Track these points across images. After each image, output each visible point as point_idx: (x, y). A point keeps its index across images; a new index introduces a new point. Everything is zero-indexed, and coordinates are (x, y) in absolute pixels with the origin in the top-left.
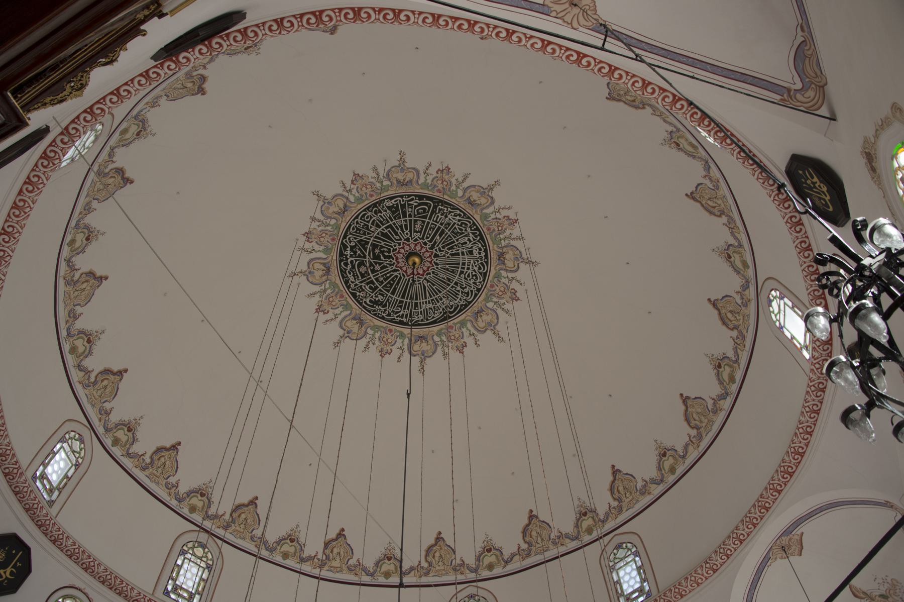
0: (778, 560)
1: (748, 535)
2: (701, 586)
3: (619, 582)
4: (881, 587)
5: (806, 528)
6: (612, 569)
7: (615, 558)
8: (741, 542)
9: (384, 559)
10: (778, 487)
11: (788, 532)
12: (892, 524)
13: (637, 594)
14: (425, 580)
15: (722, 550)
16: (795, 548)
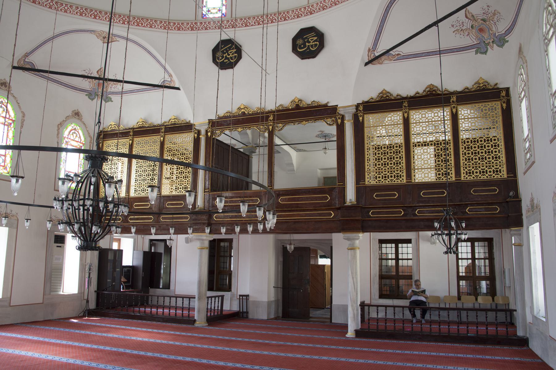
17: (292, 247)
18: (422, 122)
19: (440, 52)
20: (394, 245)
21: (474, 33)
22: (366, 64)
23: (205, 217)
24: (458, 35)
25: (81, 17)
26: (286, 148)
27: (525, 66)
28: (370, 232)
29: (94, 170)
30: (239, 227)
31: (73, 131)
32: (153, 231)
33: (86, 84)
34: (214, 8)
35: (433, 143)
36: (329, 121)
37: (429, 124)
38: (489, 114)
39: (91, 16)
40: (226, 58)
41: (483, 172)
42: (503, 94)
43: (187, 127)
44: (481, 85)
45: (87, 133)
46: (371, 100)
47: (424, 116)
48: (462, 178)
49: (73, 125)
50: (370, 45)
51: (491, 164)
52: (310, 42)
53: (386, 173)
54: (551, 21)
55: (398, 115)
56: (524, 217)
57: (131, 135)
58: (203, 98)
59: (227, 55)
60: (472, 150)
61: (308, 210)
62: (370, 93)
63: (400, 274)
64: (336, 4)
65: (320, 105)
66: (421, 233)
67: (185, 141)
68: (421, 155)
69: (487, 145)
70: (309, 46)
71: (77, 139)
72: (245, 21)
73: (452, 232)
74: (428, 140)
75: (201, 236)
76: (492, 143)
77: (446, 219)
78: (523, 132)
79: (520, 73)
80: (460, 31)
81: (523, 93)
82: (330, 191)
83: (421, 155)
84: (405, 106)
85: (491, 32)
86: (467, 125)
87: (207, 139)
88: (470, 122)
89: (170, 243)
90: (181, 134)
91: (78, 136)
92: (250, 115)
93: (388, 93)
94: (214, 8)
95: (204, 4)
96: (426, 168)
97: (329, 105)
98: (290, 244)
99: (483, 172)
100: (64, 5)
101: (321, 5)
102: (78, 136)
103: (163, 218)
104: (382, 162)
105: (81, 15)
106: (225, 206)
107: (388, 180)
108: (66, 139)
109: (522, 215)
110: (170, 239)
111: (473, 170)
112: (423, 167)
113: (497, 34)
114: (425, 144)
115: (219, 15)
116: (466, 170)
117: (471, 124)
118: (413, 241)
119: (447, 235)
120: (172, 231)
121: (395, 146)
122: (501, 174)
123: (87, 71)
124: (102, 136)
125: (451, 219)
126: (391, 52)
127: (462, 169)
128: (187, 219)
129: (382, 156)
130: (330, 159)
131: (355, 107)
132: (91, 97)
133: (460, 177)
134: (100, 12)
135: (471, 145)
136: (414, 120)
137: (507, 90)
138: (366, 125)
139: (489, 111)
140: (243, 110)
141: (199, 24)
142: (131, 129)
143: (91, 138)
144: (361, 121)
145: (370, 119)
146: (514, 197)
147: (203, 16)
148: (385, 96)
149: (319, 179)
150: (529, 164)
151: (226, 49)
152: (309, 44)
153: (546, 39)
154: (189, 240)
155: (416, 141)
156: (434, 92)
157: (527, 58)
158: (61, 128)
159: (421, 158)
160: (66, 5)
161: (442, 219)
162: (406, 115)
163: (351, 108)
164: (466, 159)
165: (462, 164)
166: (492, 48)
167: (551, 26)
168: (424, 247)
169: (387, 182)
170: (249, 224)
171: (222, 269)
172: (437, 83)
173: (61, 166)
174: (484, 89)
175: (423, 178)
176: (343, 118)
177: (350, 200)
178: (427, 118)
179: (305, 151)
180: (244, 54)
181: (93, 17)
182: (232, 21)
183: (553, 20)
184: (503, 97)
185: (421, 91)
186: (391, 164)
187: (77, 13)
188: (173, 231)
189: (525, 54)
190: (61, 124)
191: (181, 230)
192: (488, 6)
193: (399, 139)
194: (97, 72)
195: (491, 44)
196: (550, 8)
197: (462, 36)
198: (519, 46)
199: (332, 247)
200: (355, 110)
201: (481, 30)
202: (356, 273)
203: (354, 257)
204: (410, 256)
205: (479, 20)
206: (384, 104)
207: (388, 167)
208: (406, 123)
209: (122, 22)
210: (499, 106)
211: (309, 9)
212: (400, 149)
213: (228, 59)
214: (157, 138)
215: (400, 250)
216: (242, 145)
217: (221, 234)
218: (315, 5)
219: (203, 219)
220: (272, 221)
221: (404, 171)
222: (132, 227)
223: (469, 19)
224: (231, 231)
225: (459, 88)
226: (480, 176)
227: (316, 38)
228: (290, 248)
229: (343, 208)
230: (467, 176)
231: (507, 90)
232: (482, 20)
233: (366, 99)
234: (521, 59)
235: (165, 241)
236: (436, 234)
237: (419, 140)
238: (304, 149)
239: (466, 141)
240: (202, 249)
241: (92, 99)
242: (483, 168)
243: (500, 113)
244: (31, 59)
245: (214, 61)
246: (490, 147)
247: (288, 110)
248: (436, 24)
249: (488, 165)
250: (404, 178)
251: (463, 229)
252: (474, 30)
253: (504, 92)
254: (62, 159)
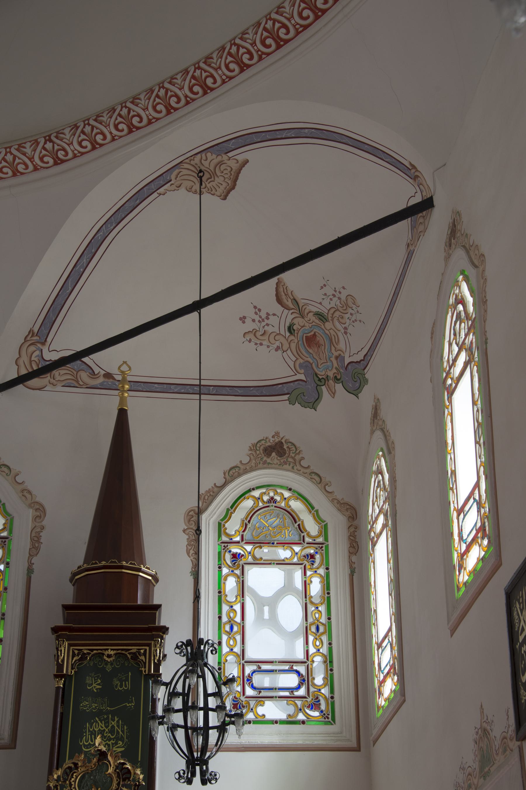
0: (182, 190)
1: (150, 122)
2: (20, 179)
4: (326, 303)
5: (257, 156)
8: (131, 129)
10: (245, 58)
11: (222, 147)
12: (400, 206)
15: (88, 129)
16: (220, 182)
19: (200, 390)
79: (375, 468)
183: (466, 335)
196: (460, 307)
198: (26, 565)
201: (311, 340)
248: (197, 306)
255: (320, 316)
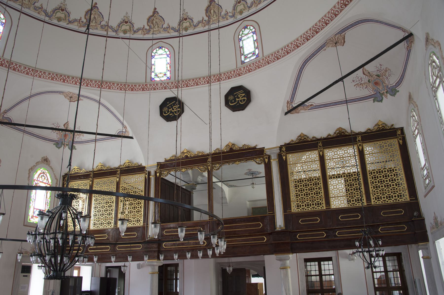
3: (242, 47)
6: (240, 40)
7: (242, 34)
9: (236, 4)
13: (251, 55)
14: (147, 36)
17: (231, 269)
18: (335, 159)
19: (346, 102)
20: (317, 263)
21: (371, 86)
22: (286, 114)
23: (155, 246)
24: (358, 88)
25: (52, 81)
26: (220, 184)
27: (416, 109)
28: (296, 253)
29: (65, 207)
30: (190, 253)
31: (42, 174)
32: (113, 259)
33: (54, 135)
34: (161, 73)
35: (335, 176)
36: (258, 160)
37: (341, 160)
38: (389, 150)
39: (60, 80)
40: (171, 112)
41: (390, 197)
42: (399, 132)
43: (140, 169)
44: (381, 126)
45: (53, 175)
46: (292, 142)
47: (336, 153)
48: (373, 203)
49: (42, 169)
50: (288, 98)
51: (396, 190)
52: (239, 98)
53: (309, 201)
54: (437, 73)
55: (315, 153)
56: (429, 233)
57: (91, 177)
58: (154, 145)
59: (171, 109)
60: (378, 180)
61: (244, 236)
62: (291, 136)
63: (324, 288)
64: (259, 68)
65: (250, 148)
66: (339, 251)
67: (136, 182)
68: (336, 186)
69: (390, 175)
70: (238, 101)
71: (45, 181)
72: (186, 82)
73: (371, 249)
74: (352, 171)
75: (152, 262)
76: (383, 174)
77: (364, 238)
78: (420, 162)
79: (411, 115)
80: (359, 85)
81: (417, 131)
82: (262, 219)
83: (336, 186)
84: (320, 146)
85: (384, 84)
86: (372, 159)
87: (156, 179)
88: (374, 156)
89: (124, 269)
90: (134, 175)
91: (46, 178)
92: (192, 157)
93: (305, 136)
94: (161, 73)
95: (153, 70)
96: (342, 196)
97: (257, 147)
98: (229, 266)
99: (390, 197)
100: (39, 72)
101: (248, 68)
102: (46, 178)
103: (119, 248)
104: (304, 192)
105: (52, 79)
106: (185, 234)
107: (311, 207)
108: (36, 182)
109: (426, 231)
110: (124, 266)
111: (381, 195)
112: (339, 195)
113: (389, 86)
114: (339, 176)
115: (165, 78)
116: (375, 196)
117: (375, 158)
118: (333, 259)
119: (367, 252)
120: (130, 259)
121: (314, 179)
122: (404, 198)
123: (55, 124)
124: (66, 179)
125: (369, 238)
126: (306, 103)
127: (371, 195)
128: (139, 248)
129: (304, 188)
130: (259, 192)
131: (278, 149)
132: (58, 146)
133: (371, 202)
134: (68, 77)
135: (377, 175)
136: (328, 157)
137: (402, 129)
138: (288, 163)
139: (389, 147)
140: (186, 154)
141: (149, 85)
142: (91, 172)
143: (57, 180)
144: (284, 159)
145: (291, 158)
146: (418, 217)
147: (152, 79)
148: (303, 138)
149: (248, 210)
150: (429, 188)
151: (171, 105)
152: (238, 99)
153: (433, 87)
154: (141, 266)
155: (331, 174)
156: (343, 134)
157: (417, 103)
158: (32, 172)
159: (336, 188)
160: (41, 72)
161: (361, 238)
162: (321, 153)
163: (275, 149)
164: (374, 186)
165: (371, 191)
166: (386, 97)
167: (437, 77)
168: (344, 264)
169: (310, 209)
170: (194, 250)
171: (169, 291)
172: (345, 126)
173: (31, 205)
174: (383, 130)
175: (340, 205)
176: (269, 157)
177: (280, 226)
178: (339, 155)
179: (235, 186)
180: (186, 108)
181: (62, 81)
182: (175, 82)
183: (438, 73)
184: (399, 135)
185: (332, 133)
186: (302, 195)
187: (49, 78)
188: (131, 259)
189: (415, 100)
190: (31, 168)
191: (137, 257)
192: (380, 65)
193: (317, 173)
194: (64, 125)
195: (385, 94)
196: (434, 64)
197: (361, 89)
198: (408, 95)
199: (264, 268)
200: (279, 151)
201: (376, 83)
202: (289, 289)
203: (286, 275)
204: (332, 272)
205: (374, 76)
206: (303, 145)
207: (300, 198)
208: (322, 159)
209: (85, 85)
210: (397, 143)
211: (238, 72)
212: (318, 182)
213: (173, 113)
214: (114, 179)
215: (322, 266)
216: (184, 183)
217: (174, 259)
218: (242, 69)
219: (154, 248)
220: (223, 246)
221: (324, 199)
222: (94, 257)
223: (366, 75)
224: (182, 257)
225: (363, 130)
226: (387, 200)
227: (244, 94)
228: (229, 270)
229: (274, 233)
230: (376, 201)
231: (402, 129)
232: (376, 75)
233: (287, 142)
234: (412, 104)
235: (119, 267)
236: (357, 252)
237: (333, 173)
238: (235, 185)
239: (373, 172)
240: (153, 273)
241: (59, 148)
242: (377, 195)
243: (398, 148)
244: (9, 115)
245: (161, 114)
246: (393, 176)
247: (224, 152)
248: (341, 79)
249: (381, 192)
250: (324, 205)
251: (381, 246)
252: (371, 84)
253: (399, 131)
254: (32, 198)
255: (378, 76)
